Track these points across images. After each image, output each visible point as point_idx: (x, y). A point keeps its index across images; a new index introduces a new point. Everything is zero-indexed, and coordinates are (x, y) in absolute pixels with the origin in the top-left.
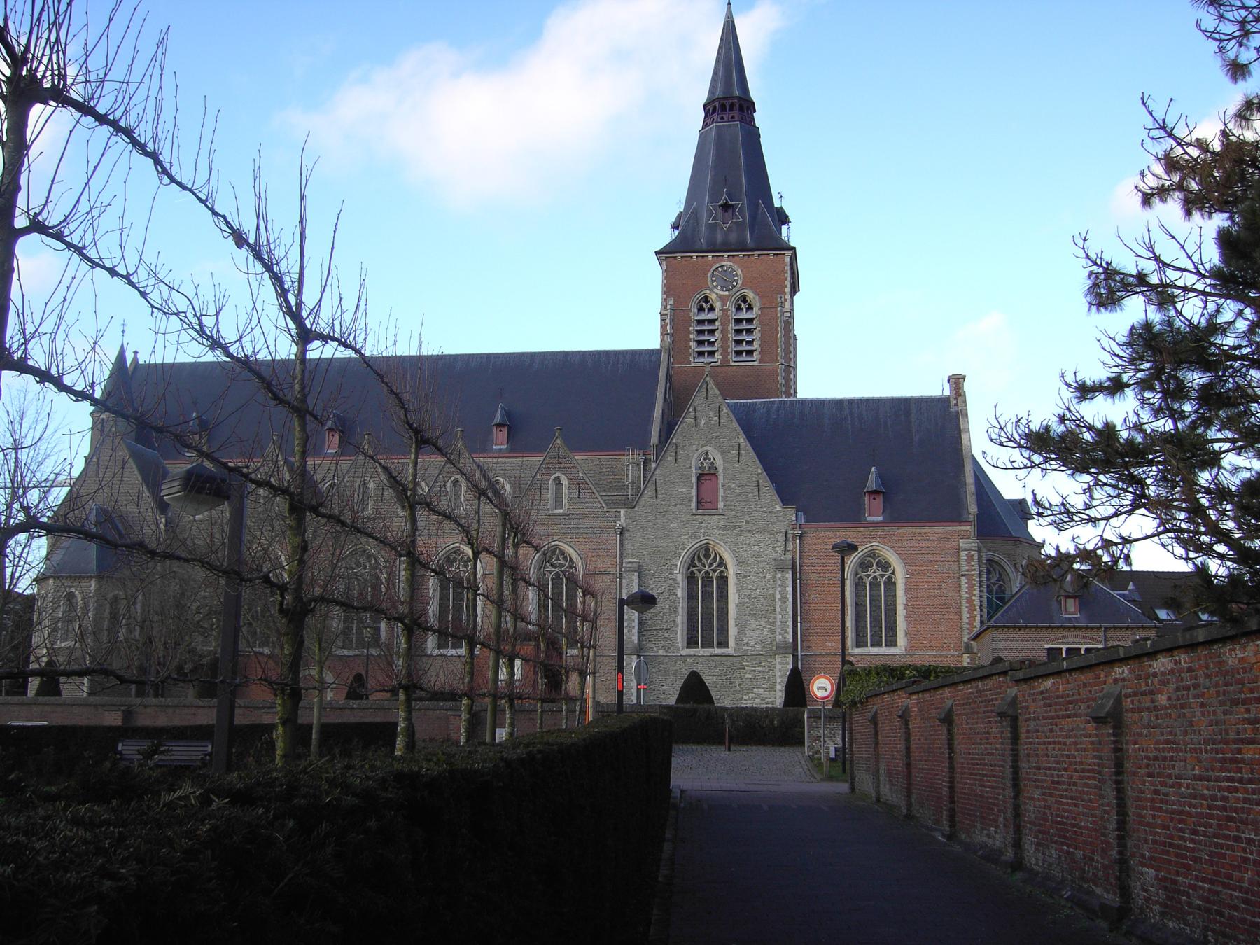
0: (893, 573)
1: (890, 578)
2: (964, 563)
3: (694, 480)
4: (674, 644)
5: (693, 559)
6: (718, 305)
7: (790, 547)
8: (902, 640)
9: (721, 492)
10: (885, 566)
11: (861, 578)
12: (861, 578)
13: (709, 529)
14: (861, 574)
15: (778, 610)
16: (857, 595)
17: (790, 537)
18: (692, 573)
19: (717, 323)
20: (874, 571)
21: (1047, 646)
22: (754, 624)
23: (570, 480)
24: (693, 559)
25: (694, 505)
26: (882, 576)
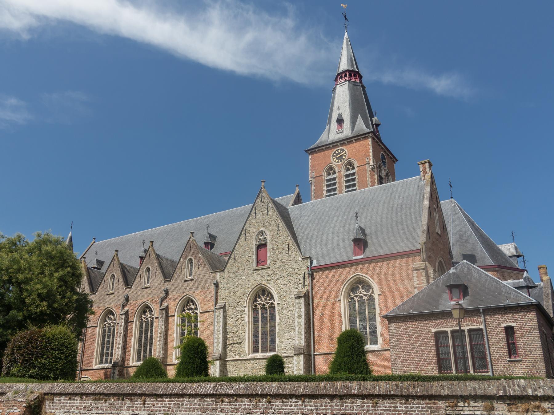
0: (373, 292)
1: (371, 296)
2: (415, 279)
3: (254, 249)
4: (243, 352)
5: (256, 298)
6: (337, 170)
7: (307, 282)
8: (380, 340)
9: (268, 254)
10: (367, 286)
11: (352, 298)
12: (352, 298)
13: (262, 278)
14: (352, 295)
15: (296, 324)
16: (350, 311)
17: (306, 276)
18: (256, 306)
19: (337, 179)
20: (361, 292)
21: (434, 330)
22: (288, 335)
23: (195, 259)
24: (256, 298)
25: (254, 264)
26: (366, 295)
